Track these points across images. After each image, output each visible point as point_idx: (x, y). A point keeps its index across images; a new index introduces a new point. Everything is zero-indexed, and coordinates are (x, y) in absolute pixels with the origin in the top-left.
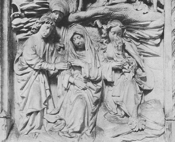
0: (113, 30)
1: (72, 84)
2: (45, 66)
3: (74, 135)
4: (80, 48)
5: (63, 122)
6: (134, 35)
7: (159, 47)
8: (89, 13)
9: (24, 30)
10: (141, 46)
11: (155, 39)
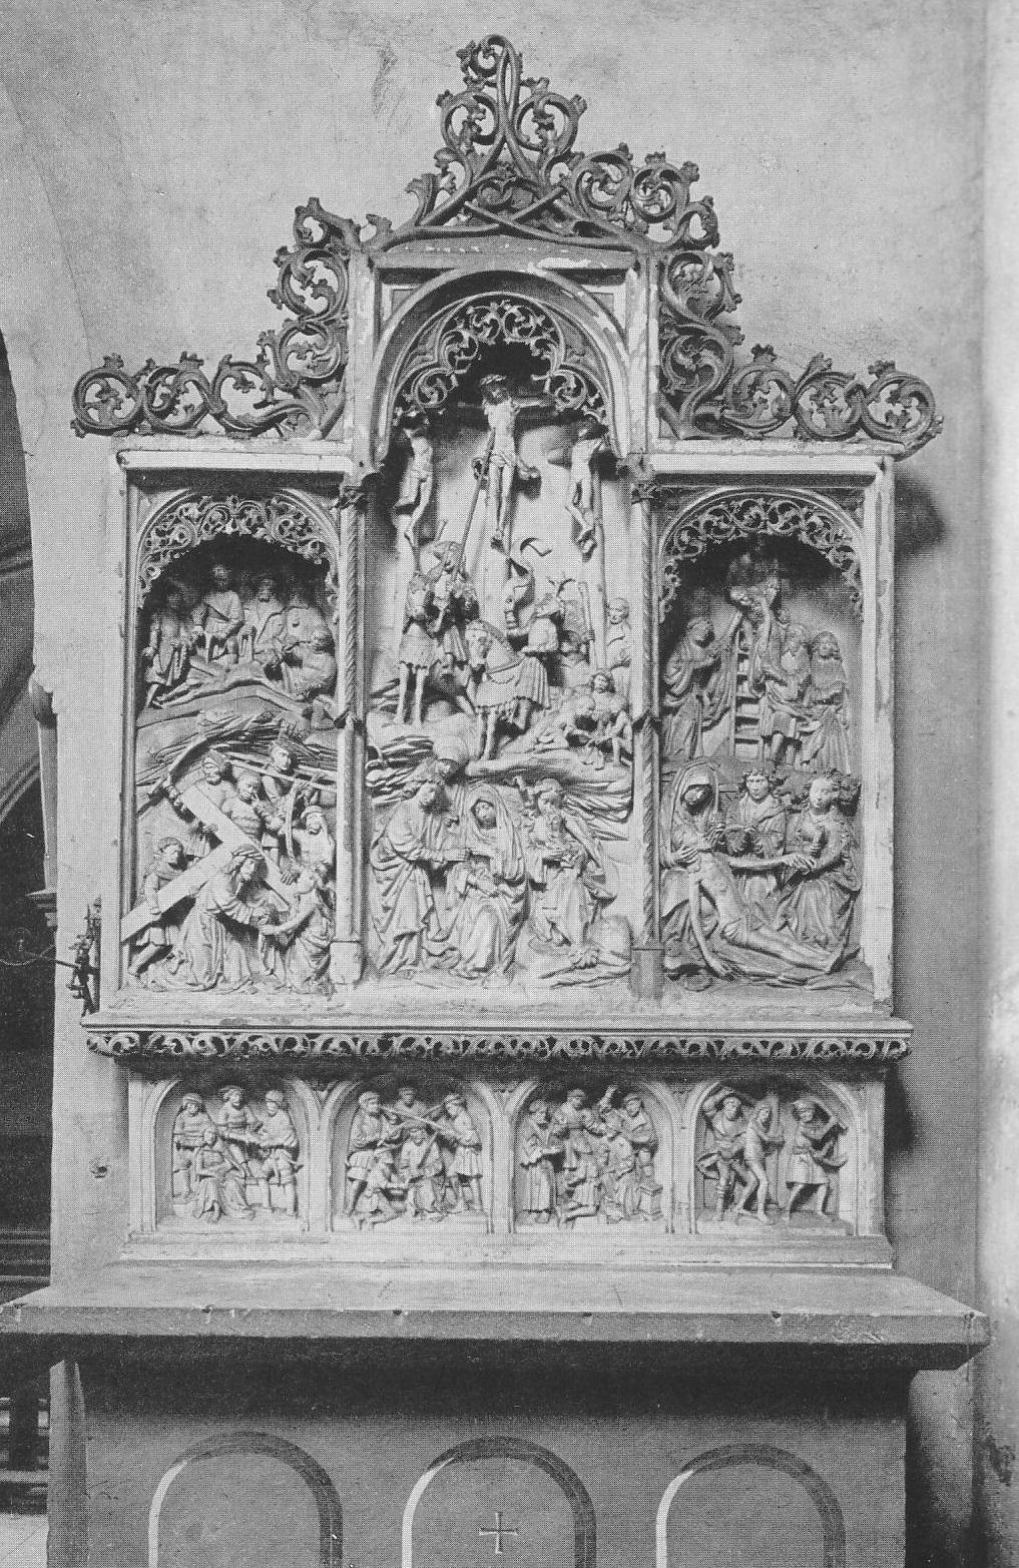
0: (544, 796)
1: (472, 886)
3: (475, 974)
5: (456, 953)
6: (583, 803)
7: (625, 825)
8: (501, 764)
9: (386, 789)
10: (596, 822)
11: (617, 810)
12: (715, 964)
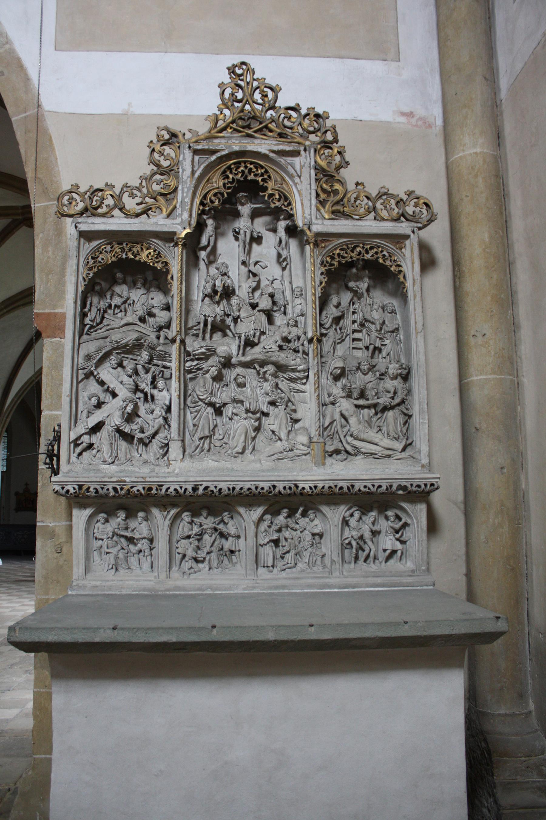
0: (268, 372)
2: (213, 400)
4: (242, 385)
6: (286, 376)
8: (248, 358)
12: (349, 448)
